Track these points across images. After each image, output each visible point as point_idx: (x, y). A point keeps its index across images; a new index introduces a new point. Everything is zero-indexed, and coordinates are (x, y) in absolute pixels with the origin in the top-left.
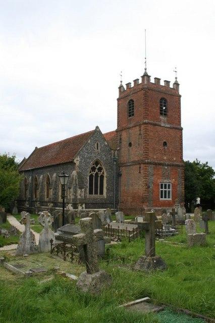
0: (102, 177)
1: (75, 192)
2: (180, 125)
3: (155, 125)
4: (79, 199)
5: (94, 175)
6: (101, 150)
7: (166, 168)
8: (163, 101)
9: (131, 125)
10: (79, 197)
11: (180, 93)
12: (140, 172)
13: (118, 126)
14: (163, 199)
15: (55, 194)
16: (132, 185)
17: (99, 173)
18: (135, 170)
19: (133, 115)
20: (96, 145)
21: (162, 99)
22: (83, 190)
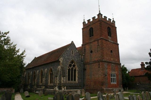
0: (75, 70)
1: (60, 79)
2: (117, 42)
3: (106, 40)
4: (63, 83)
6: (74, 54)
8: (109, 28)
9: (92, 41)
10: (62, 82)
11: (116, 26)
12: (99, 67)
13: (83, 43)
15: (46, 81)
19: (93, 35)
20: (72, 51)
21: (108, 27)
22: (65, 78)
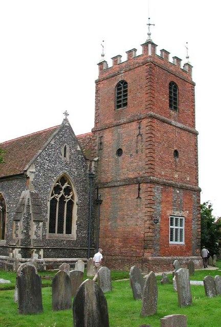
0: (71, 203)
1: (27, 228)
2: (194, 126)
3: (163, 121)
5: (58, 199)
7: (178, 192)
8: (173, 87)
10: (33, 237)
12: (139, 197)
13: (96, 123)
14: (174, 242)
16: (123, 219)
17: (66, 197)
18: (128, 195)
19: (125, 104)
22: (41, 224)
